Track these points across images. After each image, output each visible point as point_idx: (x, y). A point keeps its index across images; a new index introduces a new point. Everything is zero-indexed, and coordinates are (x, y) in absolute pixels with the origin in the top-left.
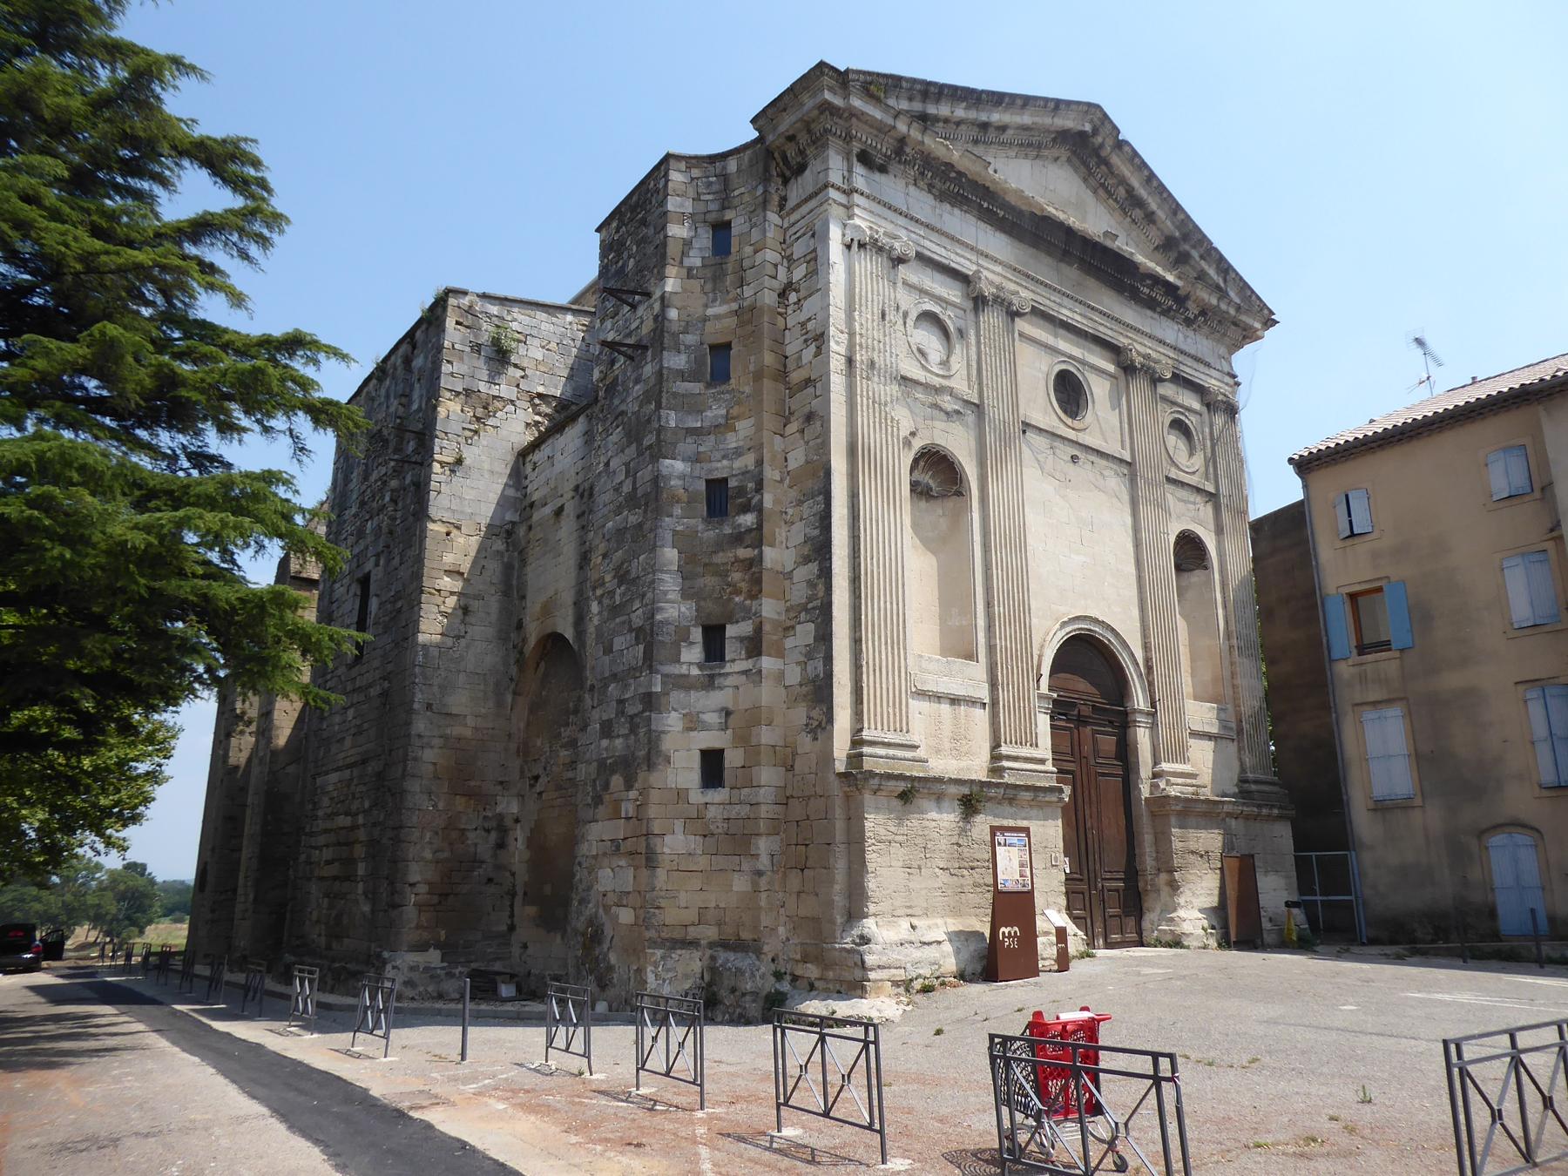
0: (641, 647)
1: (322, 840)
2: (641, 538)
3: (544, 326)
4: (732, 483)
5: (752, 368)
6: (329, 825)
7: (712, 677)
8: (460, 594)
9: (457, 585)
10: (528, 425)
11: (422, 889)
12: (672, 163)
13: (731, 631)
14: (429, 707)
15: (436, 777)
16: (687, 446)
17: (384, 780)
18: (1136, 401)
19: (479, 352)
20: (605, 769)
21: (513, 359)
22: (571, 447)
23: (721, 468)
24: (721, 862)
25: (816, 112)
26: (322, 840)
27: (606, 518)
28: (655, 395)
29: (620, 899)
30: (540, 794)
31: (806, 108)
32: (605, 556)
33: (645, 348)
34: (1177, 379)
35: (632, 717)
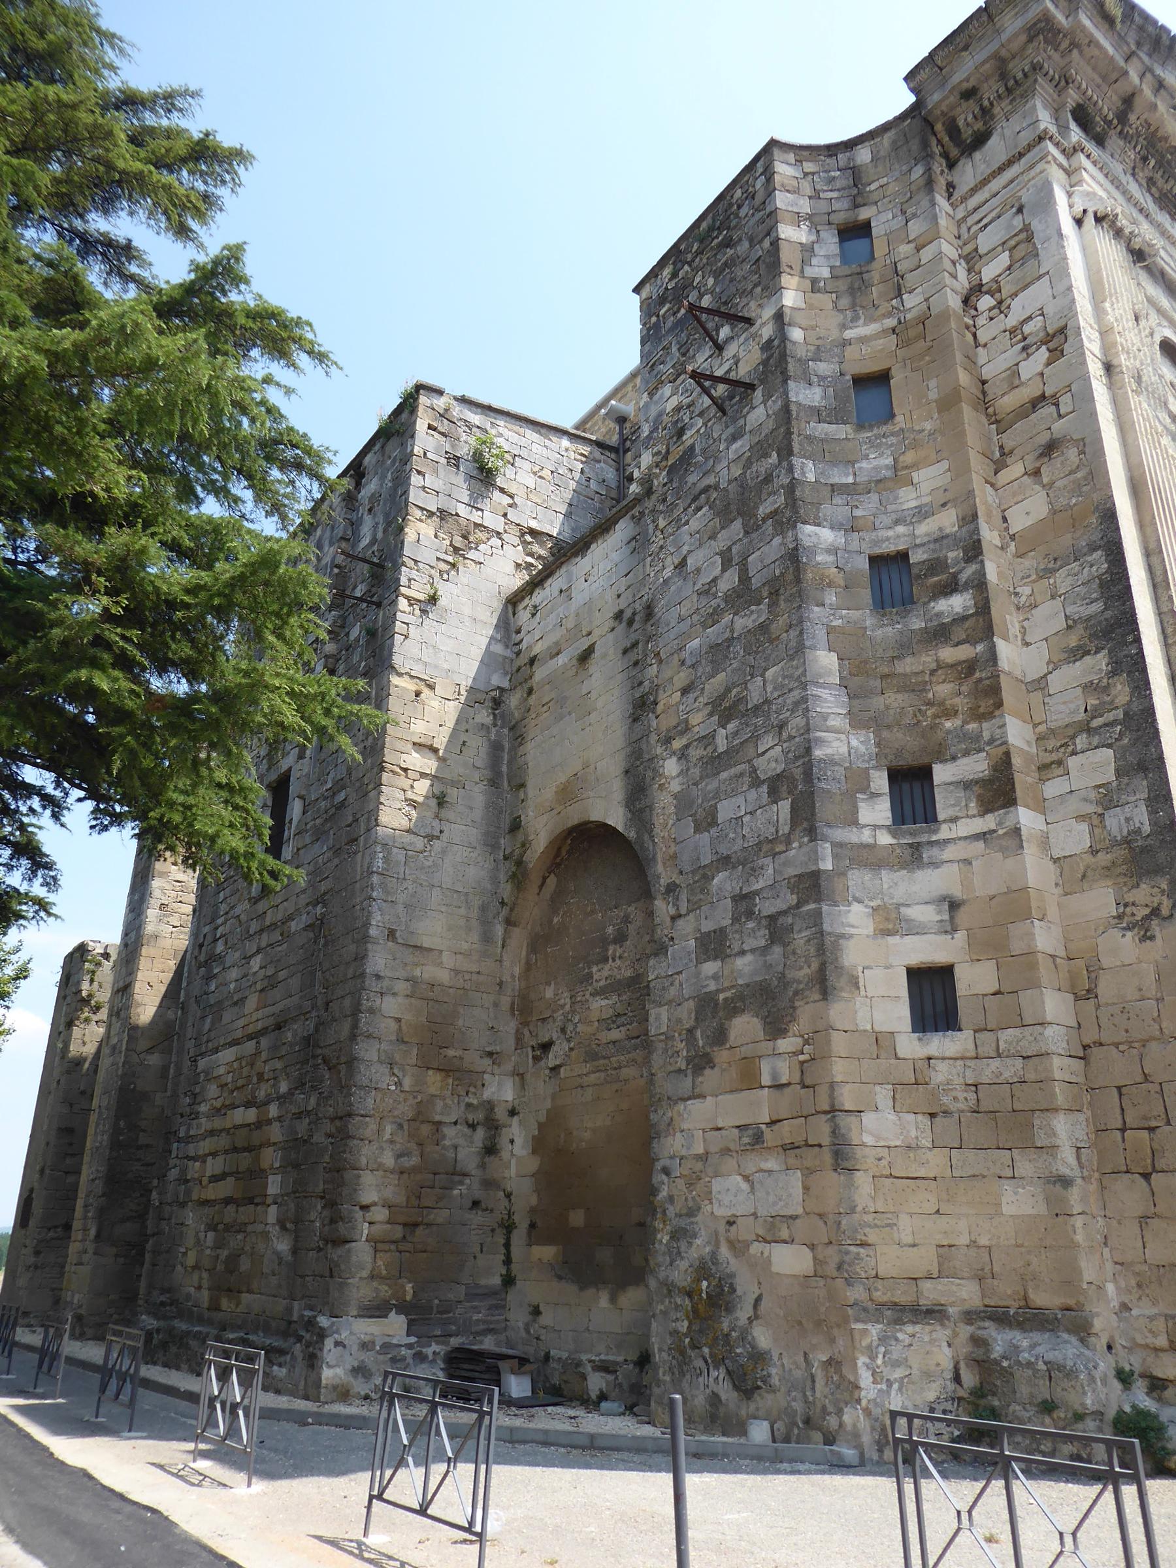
0: (785, 806)
1: (205, 1146)
2: (776, 642)
4: (914, 558)
5: (933, 395)
6: (217, 1123)
7: (916, 848)
8: (434, 778)
9: (429, 765)
10: (518, 565)
11: (380, 1214)
12: (777, 153)
13: (942, 773)
14: (391, 934)
15: (401, 1040)
16: (837, 509)
17: (317, 1050)
19: (457, 466)
20: (714, 1011)
21: (500, 481)
22: (605, 566)
23: (893, 539)
24: (971, 1161)
26: (205, 1146)
27: (685, 636)
29: (772, 1227)
30: (555, 1069)
31: (1004, 37)
32: (685, 691)
33: (751, 387)
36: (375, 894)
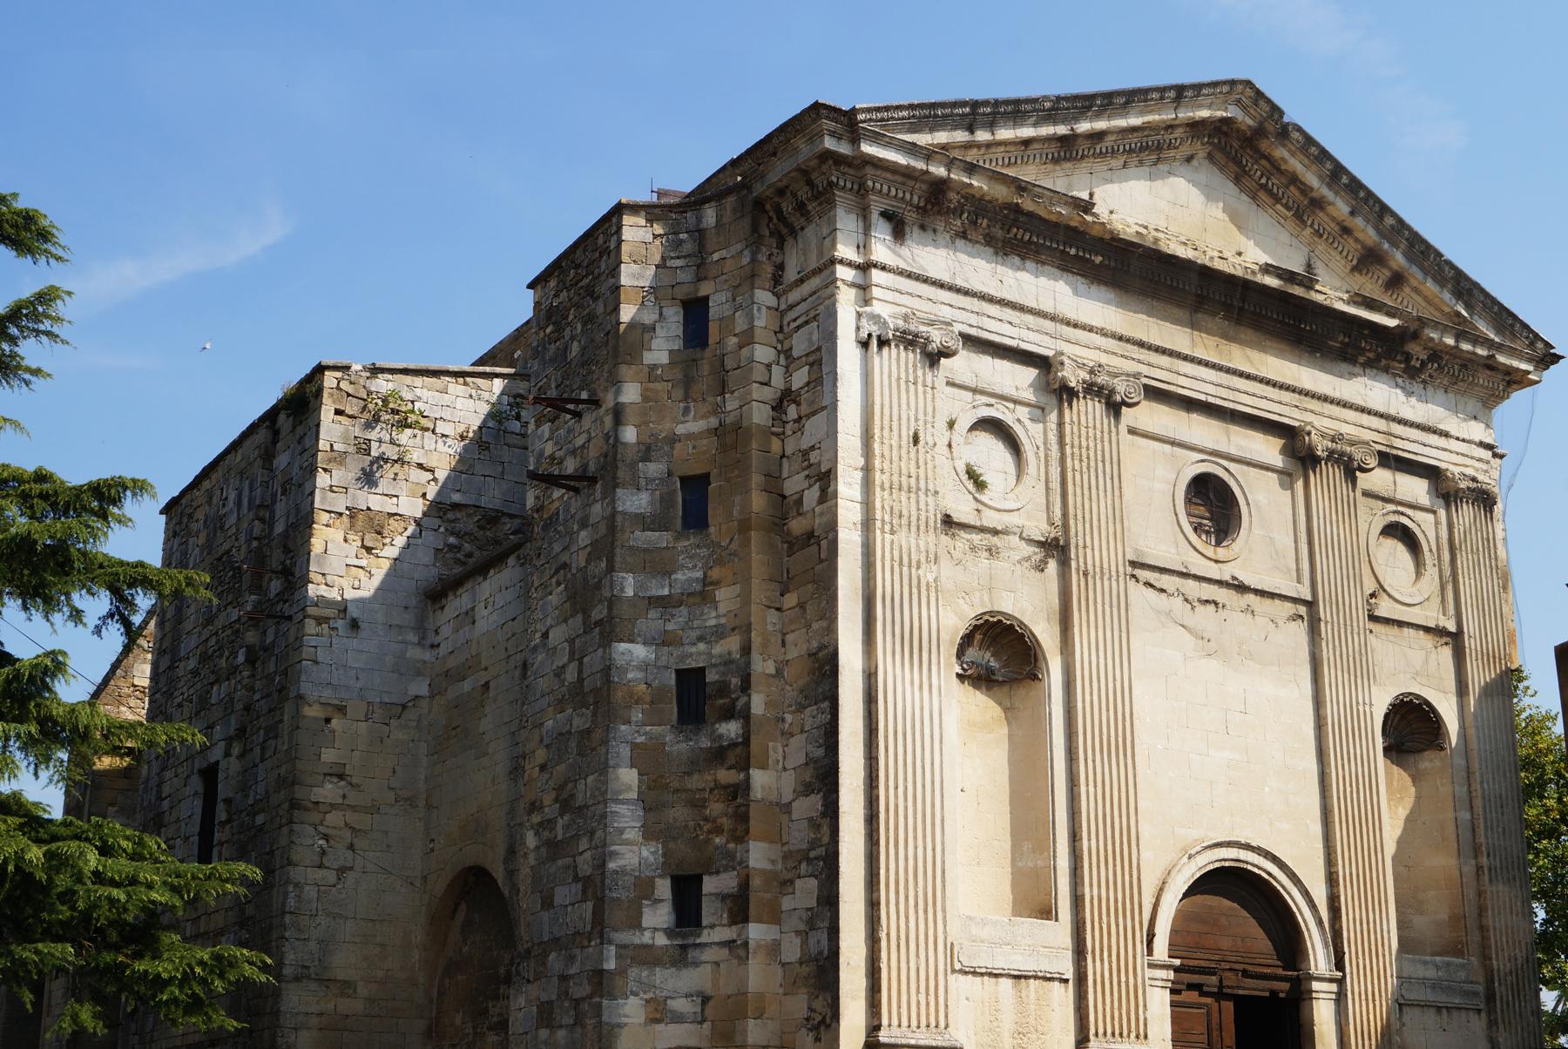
0: (590, 905)
2: (587, 750)
3: (460, 403)
4: (711, 676)
7: (684, 948)
13: (710, 885)
16: (652, 622)
23: (696, 654)
25: (814, 163)
28: (606, 548)
32: (543, 768)
33: (593, 480)
34: (1390, 460)
35: (578, 1001)
36: (287, 934)
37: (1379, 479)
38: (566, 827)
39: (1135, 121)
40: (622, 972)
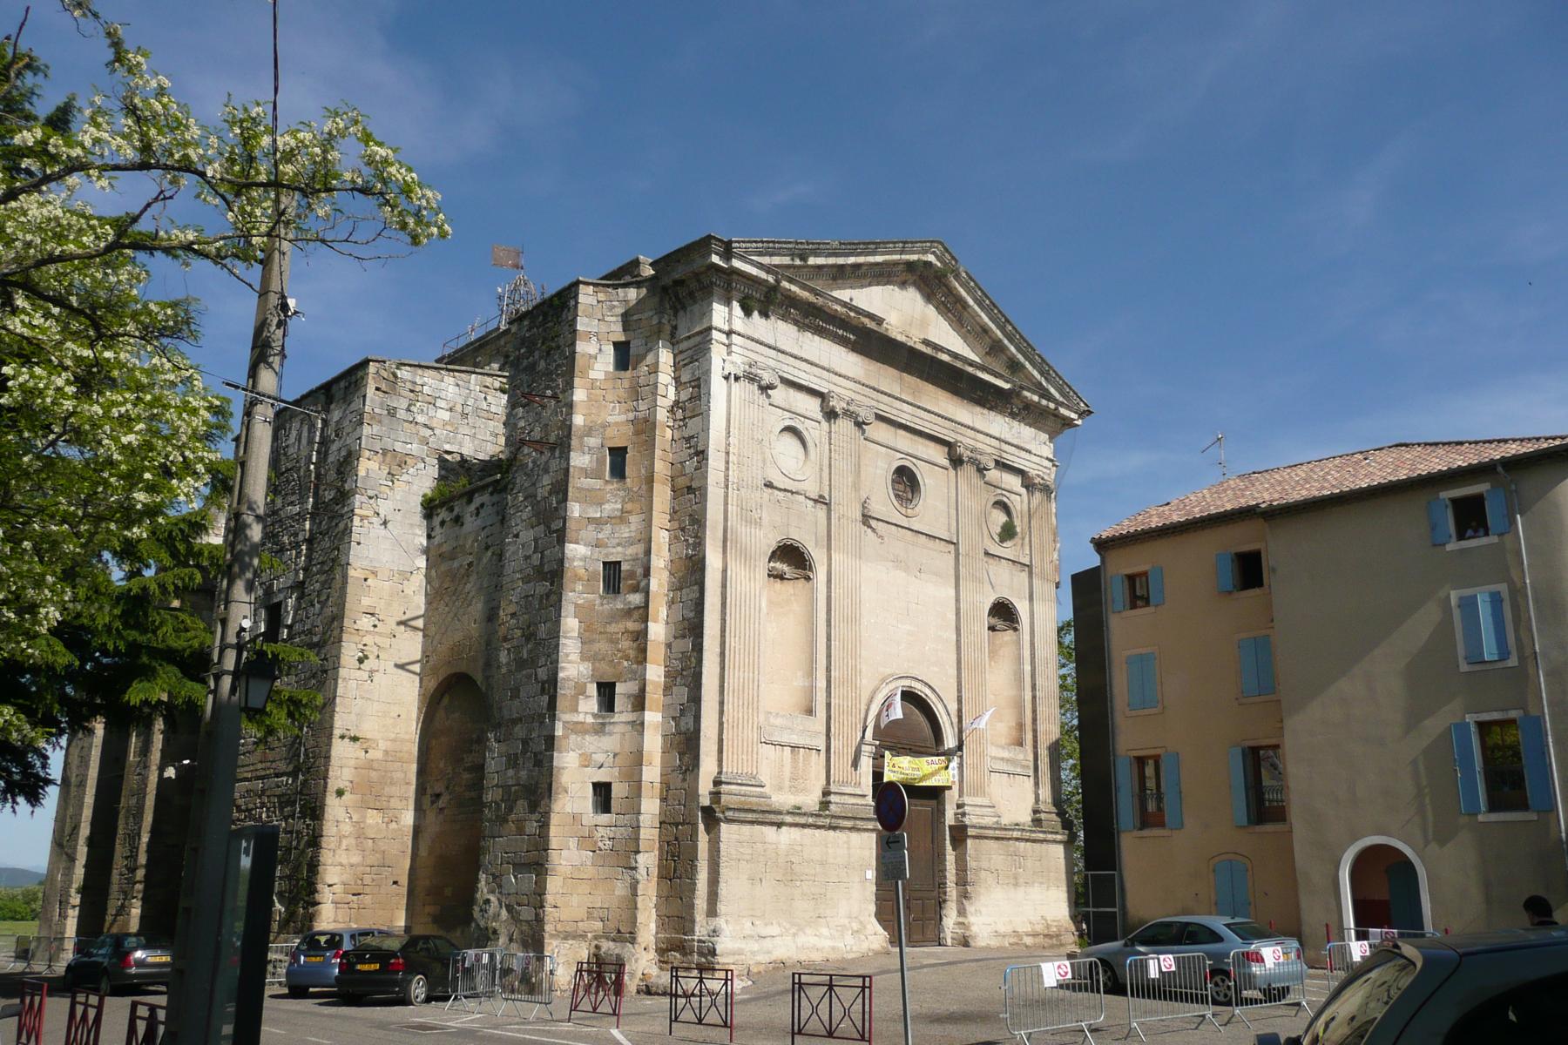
0: (546, 698)
4: (624, 567)
7: (603, 724)
11: (338, 888)
13: (619, 688)
16: (589, 533)
18: (963, 486)
34: (1002, 465)
37: (994, 474)
38: (530, 652)
39: (879, 259)
40: (566, 737)
